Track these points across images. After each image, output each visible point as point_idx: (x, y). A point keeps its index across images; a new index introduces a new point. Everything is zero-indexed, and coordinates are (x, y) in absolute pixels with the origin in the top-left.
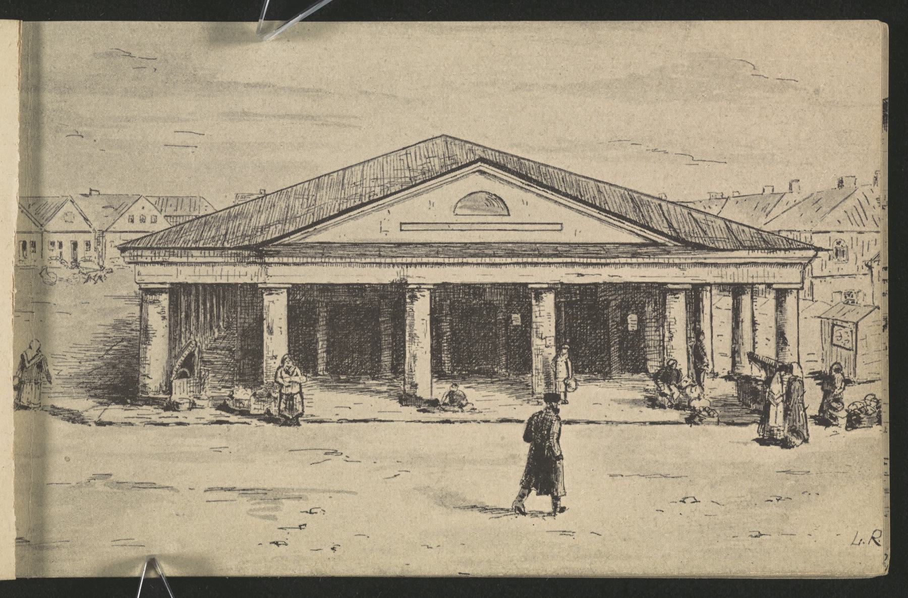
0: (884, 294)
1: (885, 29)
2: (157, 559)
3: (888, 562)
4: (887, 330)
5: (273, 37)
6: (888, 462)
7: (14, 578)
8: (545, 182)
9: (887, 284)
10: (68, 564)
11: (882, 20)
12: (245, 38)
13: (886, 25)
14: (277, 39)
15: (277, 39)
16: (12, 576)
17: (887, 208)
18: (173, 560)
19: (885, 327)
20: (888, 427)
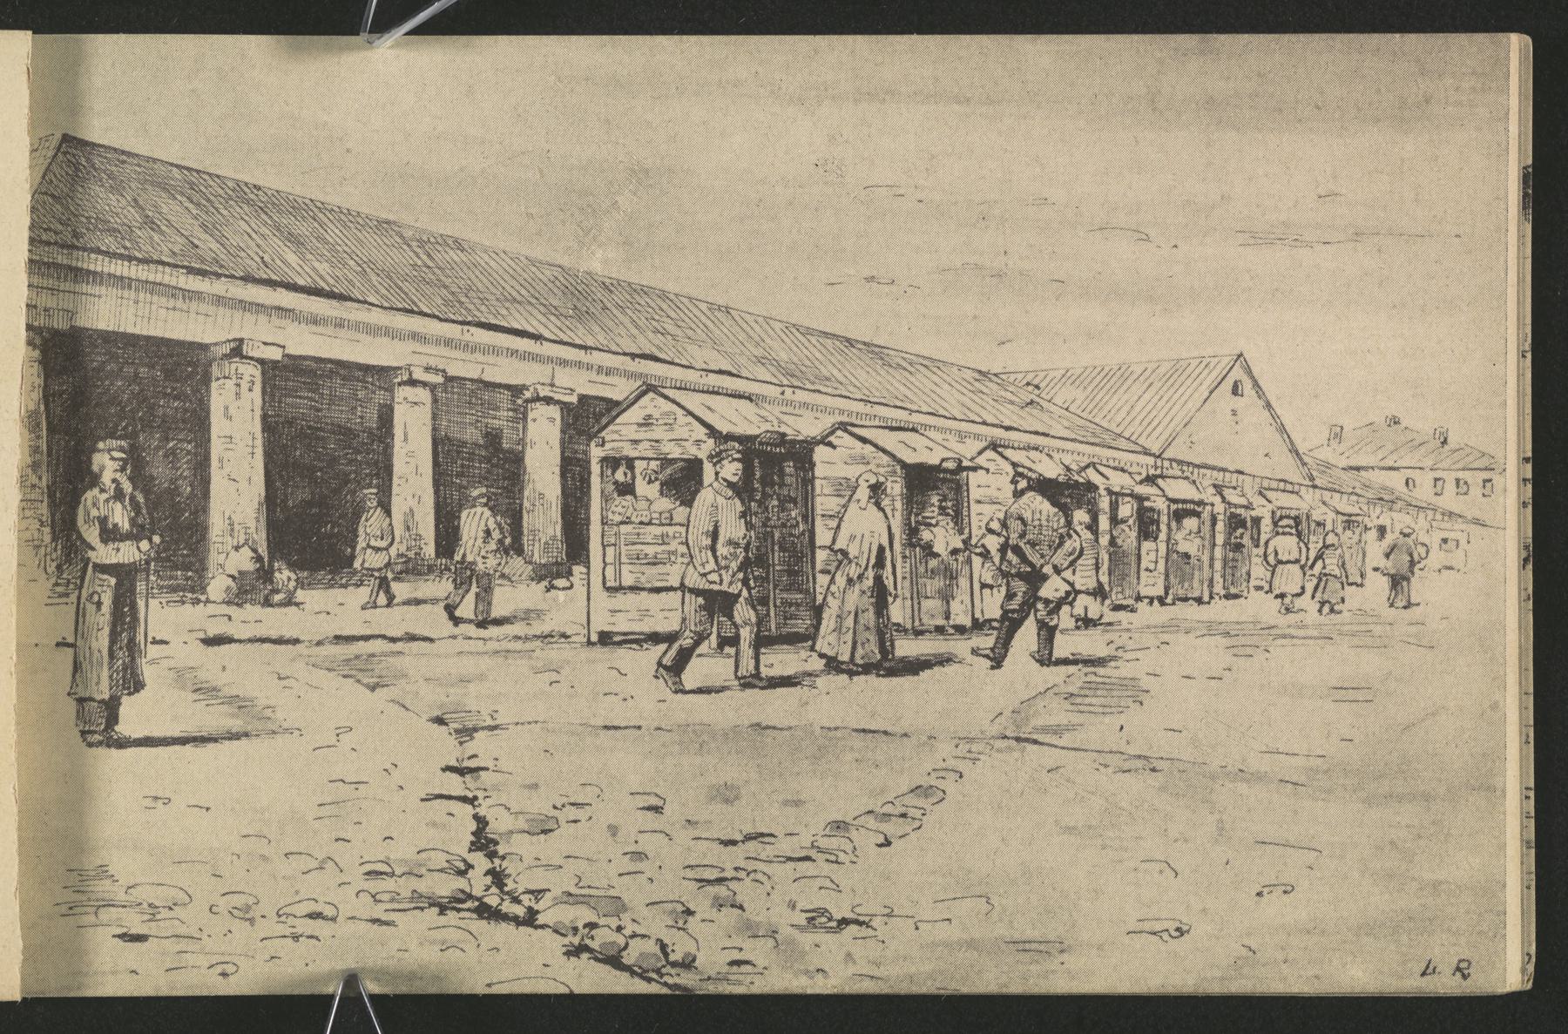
0: (1525, 505)
1: (1526, 45)
2: (361, 976)
3: (1531, 968)
4: (1530, 567)
5: (389, 43)
6: (1532, 794)
7: (18, 997)
8: (274, 277)
9: (1530, 486)
10: (118, 972)
11: (26, 28)
12: (350, 48)
13: (1528, 40)
14: (391, 47)
15: (391, 47)
16: (15, 995)
17: (1529, 355)
18: (379, 974)
19: (1526, 560)
20: (1532, 735)
